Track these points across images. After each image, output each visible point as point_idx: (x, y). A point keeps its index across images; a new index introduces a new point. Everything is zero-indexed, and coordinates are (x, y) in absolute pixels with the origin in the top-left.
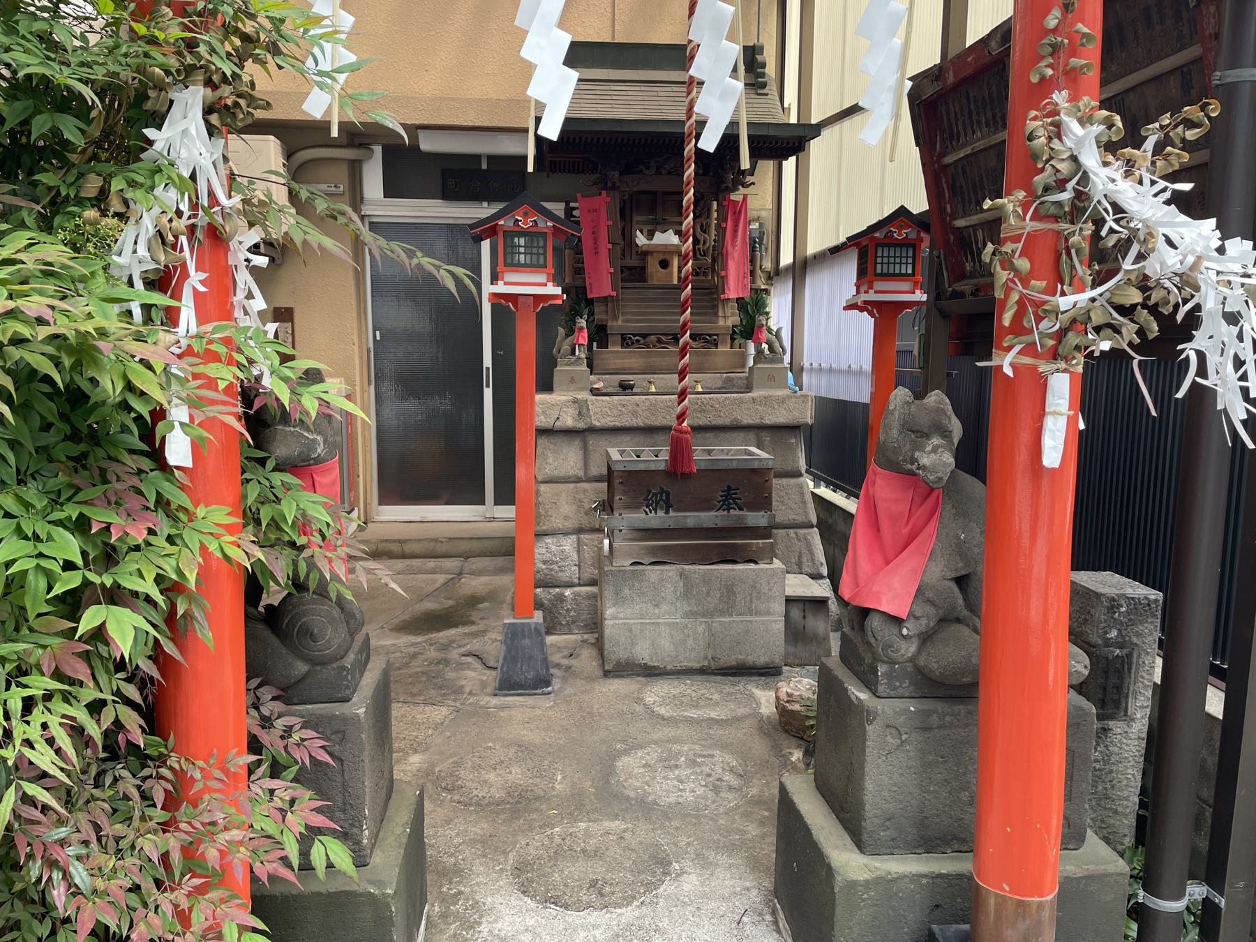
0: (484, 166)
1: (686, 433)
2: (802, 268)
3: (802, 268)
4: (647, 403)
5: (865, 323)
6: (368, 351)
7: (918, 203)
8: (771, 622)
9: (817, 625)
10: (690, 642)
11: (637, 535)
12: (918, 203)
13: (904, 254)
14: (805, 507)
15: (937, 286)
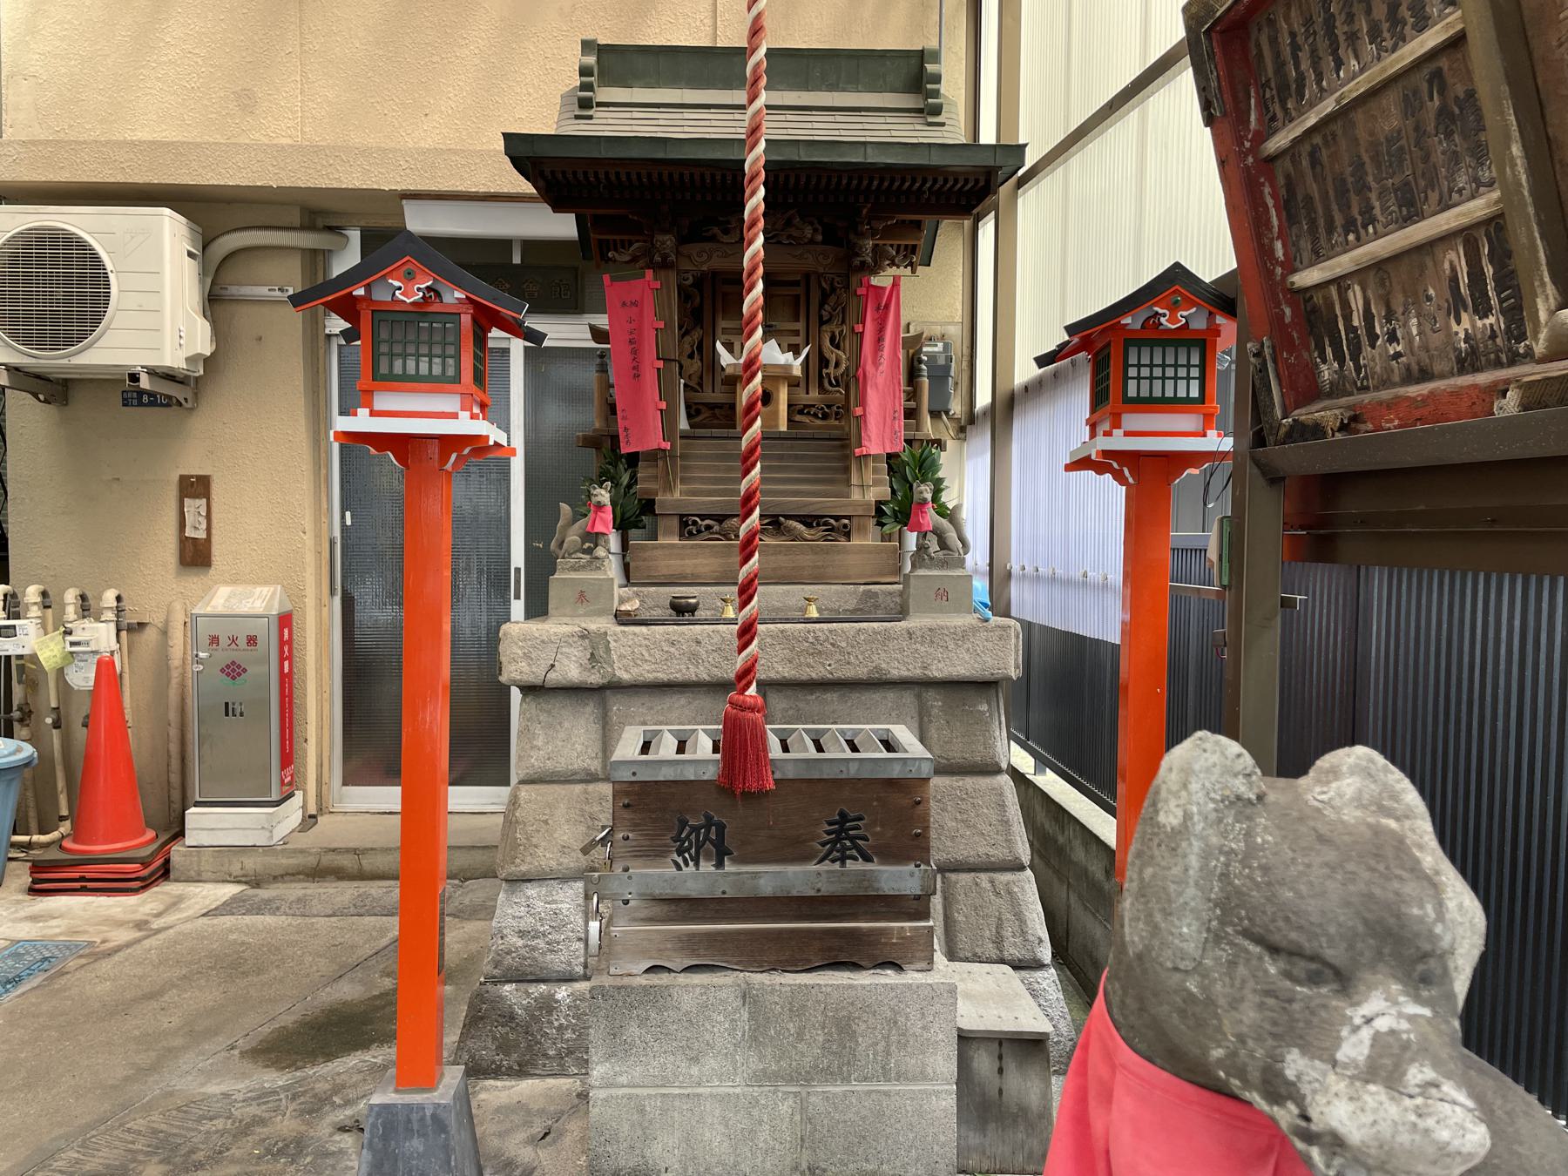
0: (517, 260)
1: (752, 709)
2: (1008, 406)
3: (1008, 406)
4: (717, 639)
5: (1108, 497)
6: (332, 543)
7: (1213, 255)
8: (929, 1094)
9: (1023, 1085)
10: (764, 1135)
11: (658, 910)
12: (1213, 255)
13: (1182, 360)
14: (1008, 832)
15: (1257, 418)
